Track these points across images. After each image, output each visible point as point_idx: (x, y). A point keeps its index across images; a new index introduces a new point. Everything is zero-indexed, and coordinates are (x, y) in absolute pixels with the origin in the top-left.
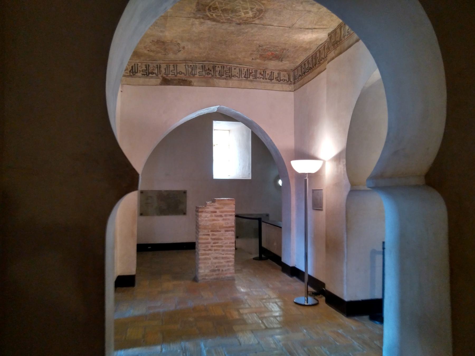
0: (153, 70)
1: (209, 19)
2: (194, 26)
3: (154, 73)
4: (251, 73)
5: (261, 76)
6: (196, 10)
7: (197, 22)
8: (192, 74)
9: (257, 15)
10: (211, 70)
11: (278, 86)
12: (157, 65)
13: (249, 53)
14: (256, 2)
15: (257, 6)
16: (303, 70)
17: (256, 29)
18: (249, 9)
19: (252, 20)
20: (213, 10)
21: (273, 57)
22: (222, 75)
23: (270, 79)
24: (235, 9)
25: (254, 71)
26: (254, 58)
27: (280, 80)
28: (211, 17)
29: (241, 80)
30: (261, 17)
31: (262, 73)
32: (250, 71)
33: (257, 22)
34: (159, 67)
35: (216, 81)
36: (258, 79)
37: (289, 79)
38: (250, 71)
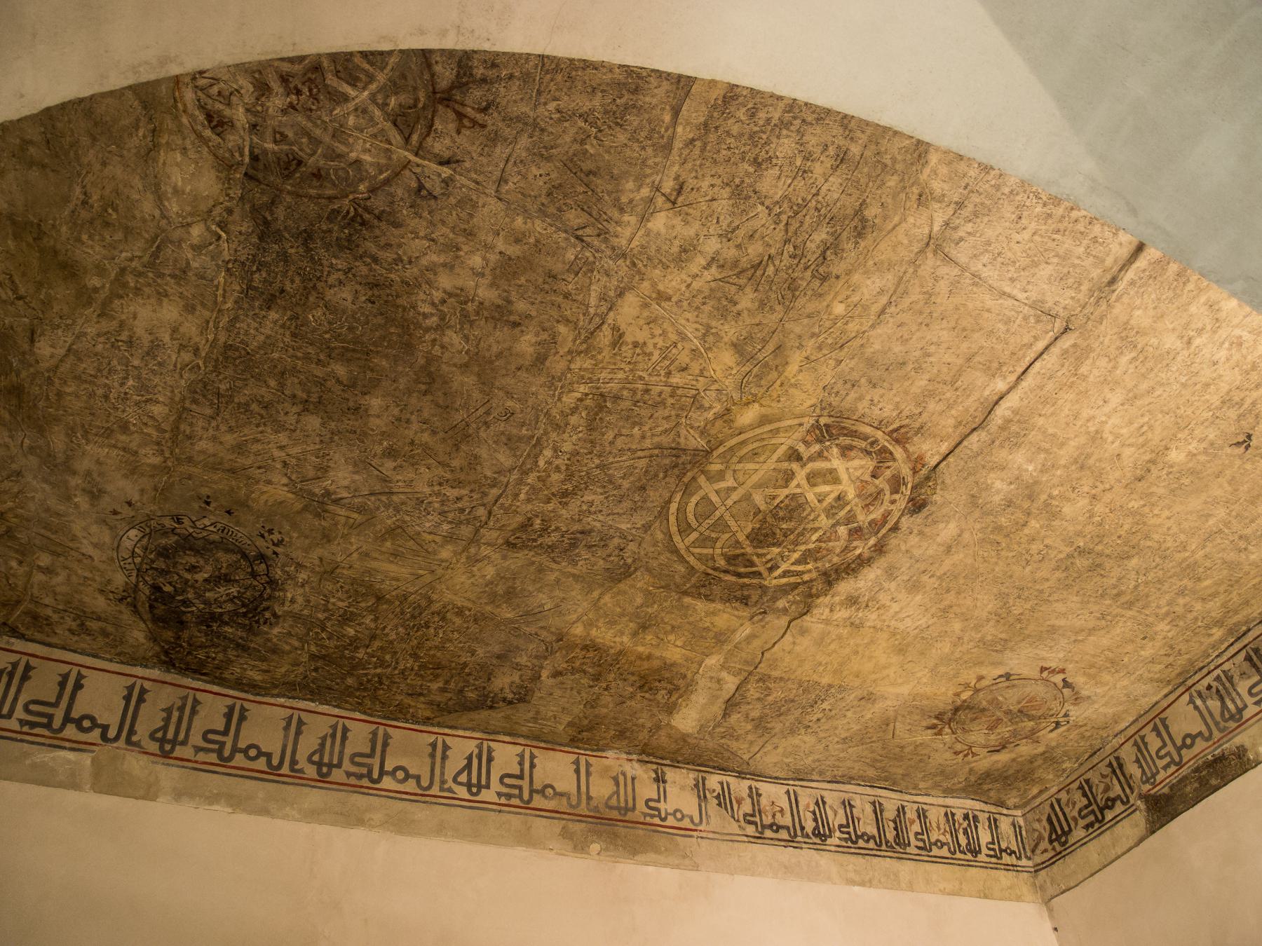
12: (1110, 765)
18: (795, 466)
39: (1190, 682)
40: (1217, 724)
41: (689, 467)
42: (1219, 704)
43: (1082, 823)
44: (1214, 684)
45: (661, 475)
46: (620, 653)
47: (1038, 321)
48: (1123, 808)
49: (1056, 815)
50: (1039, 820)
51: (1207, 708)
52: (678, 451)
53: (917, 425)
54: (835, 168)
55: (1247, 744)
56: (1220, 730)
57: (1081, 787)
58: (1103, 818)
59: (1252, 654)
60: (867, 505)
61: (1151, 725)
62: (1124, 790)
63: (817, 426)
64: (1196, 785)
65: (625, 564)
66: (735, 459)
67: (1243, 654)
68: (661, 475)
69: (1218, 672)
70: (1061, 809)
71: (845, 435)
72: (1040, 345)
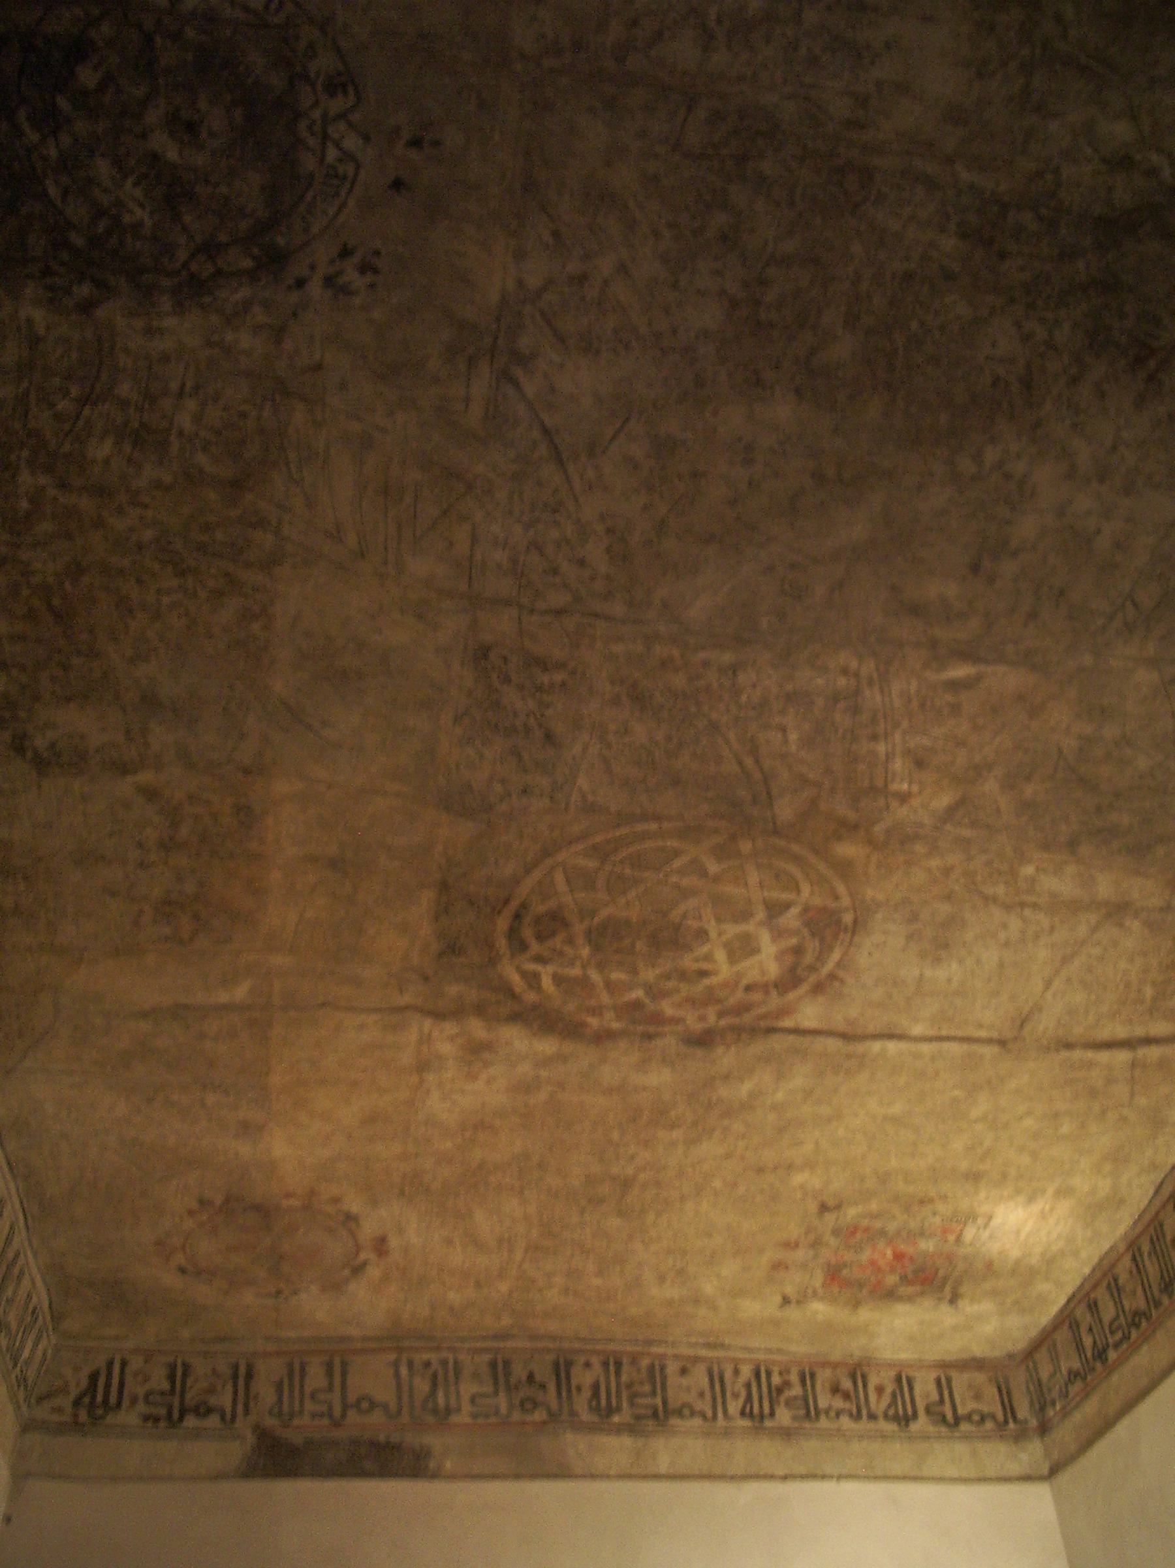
0: (211, 1390)
1: (515, 1018)
2: (430, 1077)
3: (210, 1411)
4: (780, 1391)
5: (839, 1403)
7: (445, 1040)
8: (435, 1411)
9: (809, 958)
11: (948, 1454)
12: (236, 1367)
13: (766, 1259)
14: (797, 859)
15: (806, 890)
16: (1088, 1341)
17: (799, 1078)
18: (761, 914)
19: (775, 1001)
20: (540, 938)
21: (904, 1279)
22: (610, 1411)
23: (896, 1418)
24: (675, 915)
25: (794, 1378)
26: (790, 1290)
27: (957, 1420)
28: (531, 997)
29: (727, 1433)
30: (832, 976)
31: (847, 1384)
32: (776, 1380)
33: (809, 1014)
34: (243, 1376)
35: (575, 1445)
36: (824, 1423)
38: (776, 1380)
57: (172, 1368)
72: (983, 1034)
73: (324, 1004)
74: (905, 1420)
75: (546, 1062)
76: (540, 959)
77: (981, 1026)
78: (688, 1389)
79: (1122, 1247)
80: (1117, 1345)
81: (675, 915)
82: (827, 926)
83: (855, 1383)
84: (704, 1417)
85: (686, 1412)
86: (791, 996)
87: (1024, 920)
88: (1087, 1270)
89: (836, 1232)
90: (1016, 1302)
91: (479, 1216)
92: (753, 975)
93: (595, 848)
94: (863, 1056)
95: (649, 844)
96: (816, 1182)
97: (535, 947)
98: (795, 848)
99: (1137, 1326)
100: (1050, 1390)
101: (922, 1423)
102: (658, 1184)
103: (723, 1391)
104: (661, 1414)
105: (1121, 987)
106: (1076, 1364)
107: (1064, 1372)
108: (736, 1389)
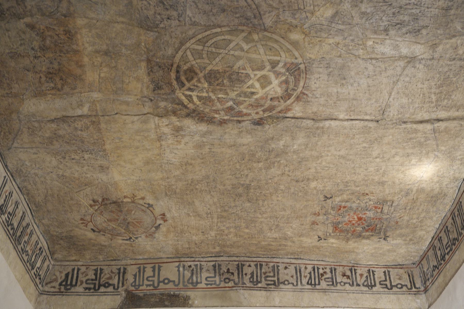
0: (110, 278)
1: (188, 115)
3: (110, 285)
4: (322, 275)
5: (345, 280)
6: (152, 87)
9: (291, 86)
10: (233, 274)
12: (119, 269)
14: (276, 41)
16: (439, 253)
17: (301, 139)
18: (268, 67)
19: (282, 105)
22: (258, 282)
23: (367, 286)
25: (328, 271)
26: (320, 234)
29: (302, 290)
31: (348, 273)
32: (321, 271)
33: (297, 110)
34: (122, 273)
36: (339, 287)
37: (413, 283)
38: (321, 271)
39: (182, 259)
40: (184, 282)
41: (250, 25)
42: (190, 275)
43: (85, 285)
44: (193, 267)
45: (237, 15)
46: (76, 52)
47: (379, 111)
48: (112, 290)
49: (257, 273)
50: (61, 272)
51: (184, 274)
52: (259, 16)
53: (309, 99)
54: (443, 9)
55: (192, 297)
56: (184, 285)
57: (96, 270)
58: (99, 289)
59: (217, 265)
60: (251, 105)
61: (153, 265)
62: (118, 283)
63: (297, 65)
64: (158, 300)
65: (157, 25)
66: (263, 43)
67: (214, 263)
68: (237, 15)
69: (198, 263)
70: (78, 273)
71: (295, 78)
72: (368, 117)
73: (116, 114)
74: (372, 286)
75: (204, 135)
76: (190, 89)
77: (366, 114)
78: (287, 274)
79: (449, 215)
80: (448, 254)
81: (235, 67)
82: (296, 71)
83: (352, 272)
84: (293, 284)
85: (286, 283)
86: (289, 102)
87: (374, 65)
88: (437, 226)
89: (333, 208)
90: (411, 240)
91: (197, 203)
92: (272, 94)
93: (199, 40)
94: (323, 128)
95: (219, 38)
96: (320, 187)
97: (188, 85)
98: (275, 36)
99: (454, 244)
100: (427, 275)
101: (378, 288)
102: (259, 187)
103: (301, 276)
104: (277, 284)
105: (421, 95)
106: (435, 264)
107: (432, 267)
108: (306, 275)
